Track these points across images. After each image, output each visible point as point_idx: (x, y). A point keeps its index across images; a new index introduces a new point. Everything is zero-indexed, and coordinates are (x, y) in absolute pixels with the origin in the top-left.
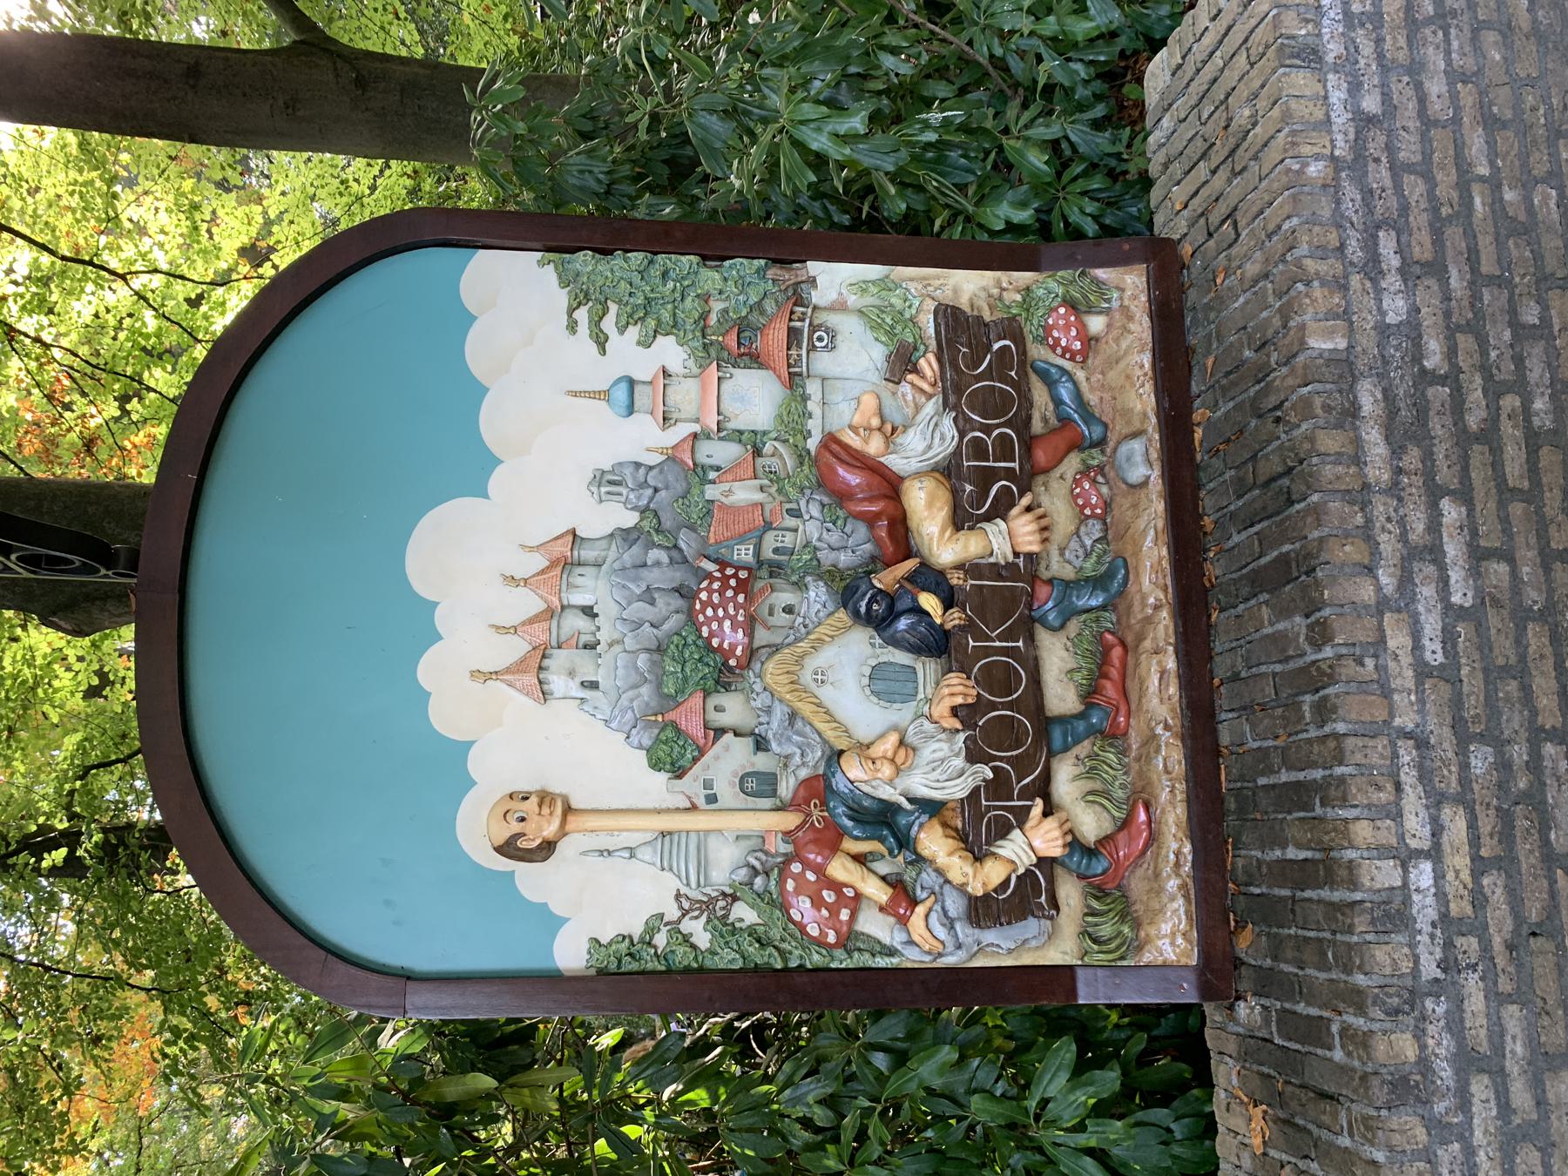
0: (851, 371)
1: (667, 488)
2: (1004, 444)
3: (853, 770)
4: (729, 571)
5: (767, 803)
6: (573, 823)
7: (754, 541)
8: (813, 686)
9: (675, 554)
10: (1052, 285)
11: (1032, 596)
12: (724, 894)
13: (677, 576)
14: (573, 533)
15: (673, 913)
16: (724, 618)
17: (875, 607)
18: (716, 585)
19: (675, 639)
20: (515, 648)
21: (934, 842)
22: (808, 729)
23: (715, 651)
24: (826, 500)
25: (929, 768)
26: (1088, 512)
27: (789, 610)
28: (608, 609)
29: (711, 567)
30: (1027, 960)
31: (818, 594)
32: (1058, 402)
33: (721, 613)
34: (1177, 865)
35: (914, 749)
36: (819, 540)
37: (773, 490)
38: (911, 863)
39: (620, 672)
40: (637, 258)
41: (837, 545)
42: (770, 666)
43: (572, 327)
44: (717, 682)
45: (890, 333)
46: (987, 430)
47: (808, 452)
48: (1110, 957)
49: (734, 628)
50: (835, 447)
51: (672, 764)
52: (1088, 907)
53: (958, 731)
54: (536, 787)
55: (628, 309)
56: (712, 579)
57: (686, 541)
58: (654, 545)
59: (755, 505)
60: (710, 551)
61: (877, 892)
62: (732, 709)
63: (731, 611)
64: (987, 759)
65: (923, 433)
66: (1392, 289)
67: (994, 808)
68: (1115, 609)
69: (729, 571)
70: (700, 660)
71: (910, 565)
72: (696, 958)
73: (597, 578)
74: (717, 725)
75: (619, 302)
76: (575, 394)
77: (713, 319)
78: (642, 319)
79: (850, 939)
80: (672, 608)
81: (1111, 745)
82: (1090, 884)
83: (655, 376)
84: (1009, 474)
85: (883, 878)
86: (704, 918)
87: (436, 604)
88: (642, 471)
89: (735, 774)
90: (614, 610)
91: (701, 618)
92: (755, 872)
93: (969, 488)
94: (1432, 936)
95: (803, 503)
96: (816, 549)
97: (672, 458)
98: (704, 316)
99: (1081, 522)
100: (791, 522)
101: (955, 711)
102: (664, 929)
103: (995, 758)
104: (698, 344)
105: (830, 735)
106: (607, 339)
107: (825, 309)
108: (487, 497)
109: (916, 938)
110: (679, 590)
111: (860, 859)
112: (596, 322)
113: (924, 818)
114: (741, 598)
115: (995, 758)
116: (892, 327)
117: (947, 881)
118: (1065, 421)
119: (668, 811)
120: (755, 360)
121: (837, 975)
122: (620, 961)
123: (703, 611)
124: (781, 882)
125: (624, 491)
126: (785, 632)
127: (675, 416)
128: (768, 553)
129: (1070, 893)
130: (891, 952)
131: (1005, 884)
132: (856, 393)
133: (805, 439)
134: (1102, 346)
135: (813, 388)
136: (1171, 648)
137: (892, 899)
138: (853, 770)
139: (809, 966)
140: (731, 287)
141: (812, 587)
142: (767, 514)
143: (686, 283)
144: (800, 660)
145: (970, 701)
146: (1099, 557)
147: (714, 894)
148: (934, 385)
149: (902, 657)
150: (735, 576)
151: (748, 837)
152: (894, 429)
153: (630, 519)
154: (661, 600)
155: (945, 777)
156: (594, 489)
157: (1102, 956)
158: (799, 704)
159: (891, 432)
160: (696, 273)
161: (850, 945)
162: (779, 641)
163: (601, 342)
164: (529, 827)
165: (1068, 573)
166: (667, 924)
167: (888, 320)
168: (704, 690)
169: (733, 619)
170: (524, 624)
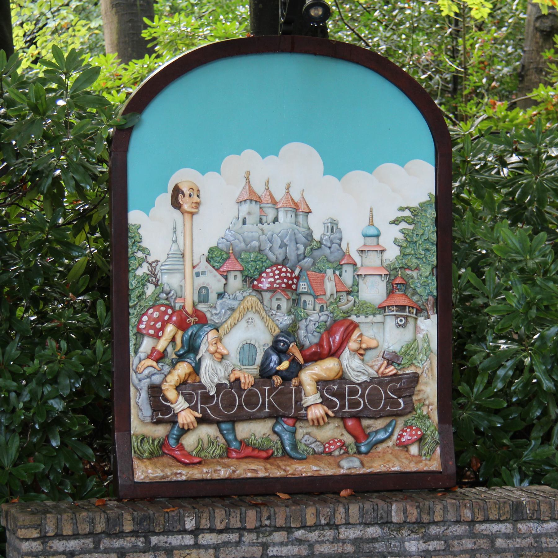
0: (387, 335)
1: (331, 252)
2: (354, 404)
3: (212, 335)
4: (295, 281)
5: (196, 299)
6: (187, 216)
7: (309, 291)
8: (246, 318)
9: (302, 257)
10: (432, 429)
11: (288, 417)
12: (158, 280)
13: (292, 257)
14: (310, 212)
15: (151, 259)
16: (275, 278)
17: (282, 344)
18: (289, 275)
19: (265, 257)
20: (260, 190)
21: (183, 369)
22: (227, 316)
23: (260, 275)
24: (328, 323)
25: (214, 367)
26: (327, 445)
27: (279, 307)
28: (276, 228)
29: (297, 272)
30: (133, 411)
31: (285, 320)
32: (377, 432)
33: (277, 277)
34: (176, 474)
35: (220, 362)
36: (310, 320)
37: (332, 300)
38: (172, 362)
39: (250, 234)
40: (434, 237)
41: (308, 328)
42: (254, 299)
43: (401, 209)
44: (247, 276)
45: (406, 353)
46: (362, 396)
47: (349, 316)
48: (136, 447)
49: (270, 283)
50: (352, 327)
51: (212, 258)
52: (155, 439)
53: (229, 381)
54: (202, 201)
55: (411, 234)
56: (293, 272)
57: (308, 261)
58: (305, 247)
59: (325, 292)
60: (304, 272)
61: (160, 347)
62: (235, 283)
63: (278, 282)
64: (218, 393)
65: (360, 367)
66: (419, 545)
67: (197, 398)
68: (283, 456)
69: (295, 281)
70: (256, 268)
71: (301, 360)
72: (133, 269)
73: (291, 223)
74: (229, 276)
75: (413, 230)
76: (371, 211)
77: (408, 272)
78: (406, 240)
79: (140, 334)
80: (278, 256)
81: (223, 452)
82: (165, 440)
83: (381, 246)
84: (343, 406)
85: (165, 350)
86: (148, 272)
87: (278, 156)
88: (338, 241)
89: (208, 284)
90: (277, 231)
91: (274, 268)
92: (167, 294)
93: (336, 387)
94: (166, 542)
95: (326, 313)
96: (306, 319)
97: (345, 255)
98: (409, 268)
99: (322, 443)
100: (318, 307)
101: (238, 380)
102: (144, 256)
103: (218, 397)
104: (397, 265)
105: (225, 326)
106: (397, 225)
107: (416, 323)
108: (324, 175)
109: (143, 362)
110: (286, 259)
111: (173, 340)
112: (404, 219)
113: (193, 365)
114: (284, 286)
115: (218, 397)
116: (409, 354)
117: (166, 376)
118: (368, 436)
119: (192, 256)
120: (390, 293)
121: (437, 145)
122: (132, 238)
123: (277, 269)
124: (163, 305)
125: (329, 234)
126: (269, 306)
127: (363, 255)
128: (303, 298)
129: (160, 431)
130: (136, 352)
131: (166, 400)
132: (378, 338)
133: (356, 315)
134: (404, 453)
135: (379, 318)
136: (267, 474)
137: (159, 352)
138: (212, 335)
139: (130, 317)
140: (423, 279)
141: (289, 317)
142: (321, 297)
143: (424, 260)
144: (257, 312)
145: (242, 386)
146: (306, 450)
147: (158, 277)
148: (382, 373)
149: (259, 359)
150: (293, 283)
151: (182, 291)
152: (362, 355)
153: (317, 236)
154: (282, 251)
155: (210, 374)
156: (329, 221)
157: (136, 444)
158: (238, 312)
159: (361, 352)
160: (429, 264)
161: (138, 335)
162: (265, 303)
163: (396, 222)
164: (187, 198)
165: (299, 436)
166: (146, 257)
167: (412, 352)
168: (243, 270)
169: (274, 282)
170: (270, 193)
